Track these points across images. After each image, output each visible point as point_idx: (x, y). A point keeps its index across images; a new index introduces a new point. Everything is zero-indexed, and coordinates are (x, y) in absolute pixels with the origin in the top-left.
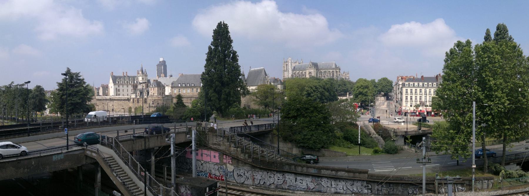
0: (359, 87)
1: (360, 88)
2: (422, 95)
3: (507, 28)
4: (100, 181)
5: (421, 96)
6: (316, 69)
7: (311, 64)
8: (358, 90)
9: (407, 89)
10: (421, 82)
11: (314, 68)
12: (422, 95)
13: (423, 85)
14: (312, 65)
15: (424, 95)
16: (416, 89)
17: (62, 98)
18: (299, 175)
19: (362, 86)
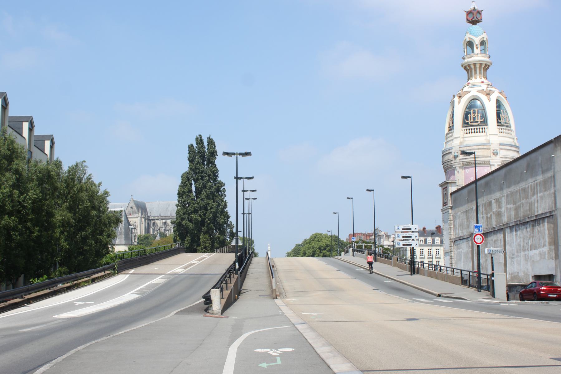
0: (322, 248)
1: (325, 249)
2: (440, 258)
3: (488, 69)
4: (261, 349)
5: (438, 260)
6: (145, 219)
7: (132, 204)
8: (320, 252)
9: (438, 248)
10: (438, 236)
11: (142, 214)
12: (440, 258)
13: (433, 241)
14: (135, 208)
15: (428, 258)
16: (438, 248)
17: (229, 258)
18: (39, 368)
19: (327, 246)
